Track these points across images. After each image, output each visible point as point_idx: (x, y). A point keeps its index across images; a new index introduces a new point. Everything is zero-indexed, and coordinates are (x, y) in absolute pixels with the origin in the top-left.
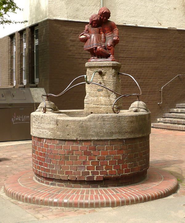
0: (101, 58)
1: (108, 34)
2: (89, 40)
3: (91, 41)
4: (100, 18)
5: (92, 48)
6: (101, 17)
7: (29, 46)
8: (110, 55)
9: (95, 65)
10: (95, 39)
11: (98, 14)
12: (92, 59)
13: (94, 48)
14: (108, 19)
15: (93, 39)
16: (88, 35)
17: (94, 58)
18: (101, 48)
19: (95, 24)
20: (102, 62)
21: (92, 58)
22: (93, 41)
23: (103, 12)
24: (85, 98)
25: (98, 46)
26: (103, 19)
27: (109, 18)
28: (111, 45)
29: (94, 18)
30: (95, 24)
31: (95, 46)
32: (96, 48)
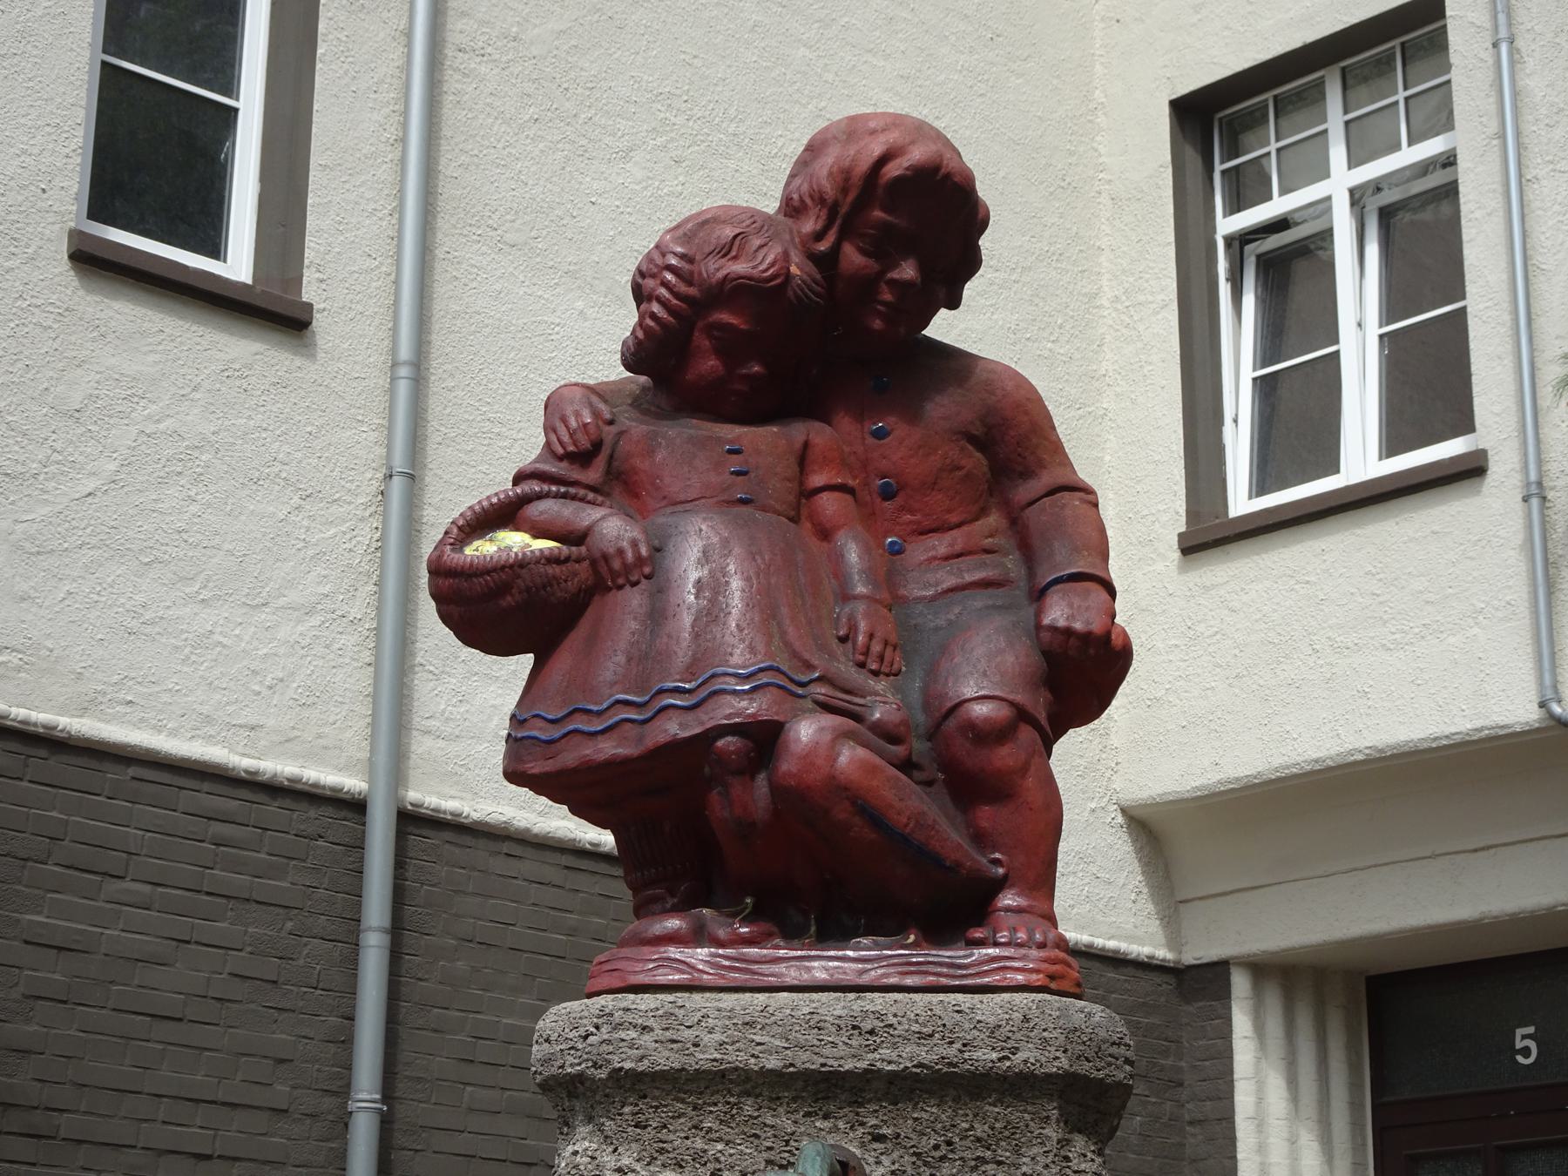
0: (833, 933)
1: (941, 544)
2: (634, 600)
3: (658, 615)
4: (826, 263)
5: (674, 728)
6: (836, 248)
7: (654, 914)
8: (999, 885)
9: (737, 1057)
10: (736, 584)
11: (792, 208)
12: (672, 939)
13: (727, 743)
14: (943, 327)
15: (713, 588)
16: (613, 528)
17: (697, 936)
18: (861, 752)
19: (730, 346)
20: (877, 1001)
21: (674, 923)
22: (711, 614)
23: (893, 170)
24: (640, 758)
25: (792, 690)
26: (867, 285)
27: (954, 303)
28: (1022, 715)
29: (727, 250)
30: (730, 346)
31: (750, 708)
32: (765, 738)
